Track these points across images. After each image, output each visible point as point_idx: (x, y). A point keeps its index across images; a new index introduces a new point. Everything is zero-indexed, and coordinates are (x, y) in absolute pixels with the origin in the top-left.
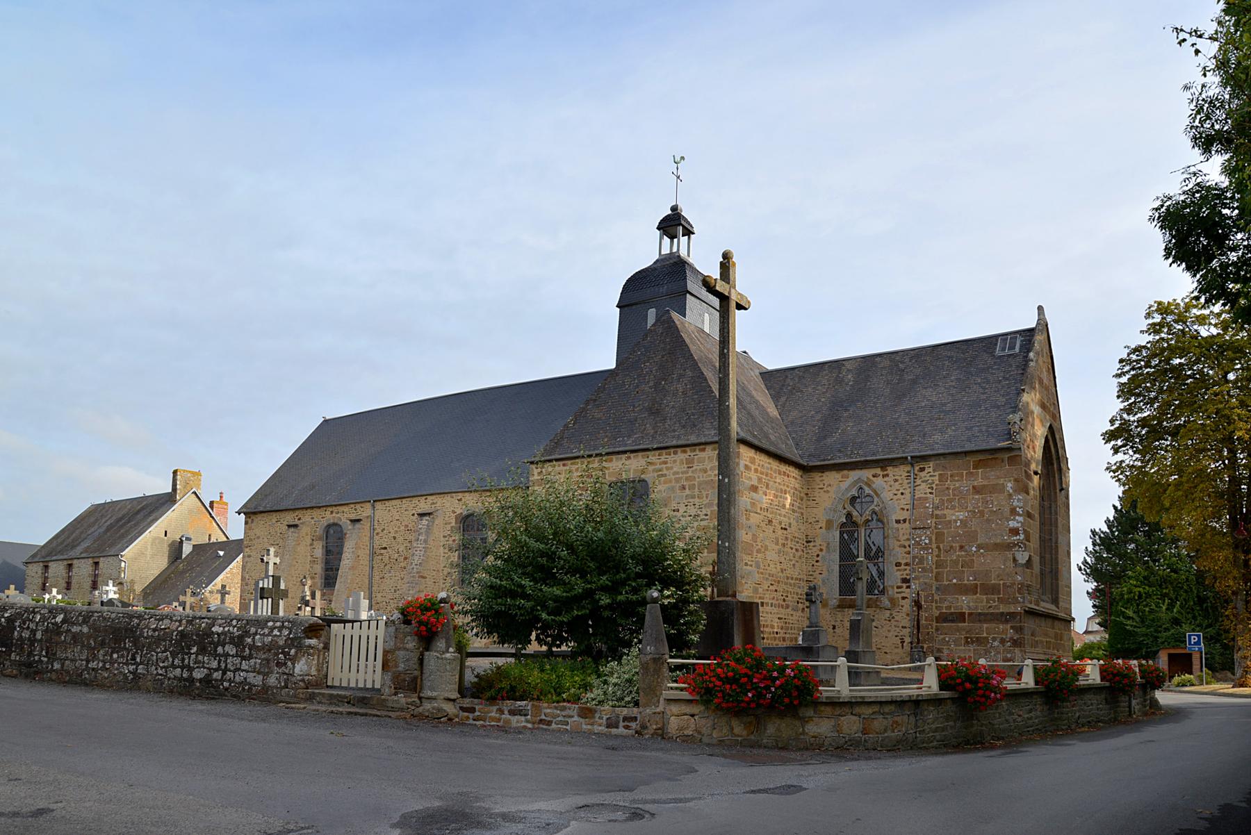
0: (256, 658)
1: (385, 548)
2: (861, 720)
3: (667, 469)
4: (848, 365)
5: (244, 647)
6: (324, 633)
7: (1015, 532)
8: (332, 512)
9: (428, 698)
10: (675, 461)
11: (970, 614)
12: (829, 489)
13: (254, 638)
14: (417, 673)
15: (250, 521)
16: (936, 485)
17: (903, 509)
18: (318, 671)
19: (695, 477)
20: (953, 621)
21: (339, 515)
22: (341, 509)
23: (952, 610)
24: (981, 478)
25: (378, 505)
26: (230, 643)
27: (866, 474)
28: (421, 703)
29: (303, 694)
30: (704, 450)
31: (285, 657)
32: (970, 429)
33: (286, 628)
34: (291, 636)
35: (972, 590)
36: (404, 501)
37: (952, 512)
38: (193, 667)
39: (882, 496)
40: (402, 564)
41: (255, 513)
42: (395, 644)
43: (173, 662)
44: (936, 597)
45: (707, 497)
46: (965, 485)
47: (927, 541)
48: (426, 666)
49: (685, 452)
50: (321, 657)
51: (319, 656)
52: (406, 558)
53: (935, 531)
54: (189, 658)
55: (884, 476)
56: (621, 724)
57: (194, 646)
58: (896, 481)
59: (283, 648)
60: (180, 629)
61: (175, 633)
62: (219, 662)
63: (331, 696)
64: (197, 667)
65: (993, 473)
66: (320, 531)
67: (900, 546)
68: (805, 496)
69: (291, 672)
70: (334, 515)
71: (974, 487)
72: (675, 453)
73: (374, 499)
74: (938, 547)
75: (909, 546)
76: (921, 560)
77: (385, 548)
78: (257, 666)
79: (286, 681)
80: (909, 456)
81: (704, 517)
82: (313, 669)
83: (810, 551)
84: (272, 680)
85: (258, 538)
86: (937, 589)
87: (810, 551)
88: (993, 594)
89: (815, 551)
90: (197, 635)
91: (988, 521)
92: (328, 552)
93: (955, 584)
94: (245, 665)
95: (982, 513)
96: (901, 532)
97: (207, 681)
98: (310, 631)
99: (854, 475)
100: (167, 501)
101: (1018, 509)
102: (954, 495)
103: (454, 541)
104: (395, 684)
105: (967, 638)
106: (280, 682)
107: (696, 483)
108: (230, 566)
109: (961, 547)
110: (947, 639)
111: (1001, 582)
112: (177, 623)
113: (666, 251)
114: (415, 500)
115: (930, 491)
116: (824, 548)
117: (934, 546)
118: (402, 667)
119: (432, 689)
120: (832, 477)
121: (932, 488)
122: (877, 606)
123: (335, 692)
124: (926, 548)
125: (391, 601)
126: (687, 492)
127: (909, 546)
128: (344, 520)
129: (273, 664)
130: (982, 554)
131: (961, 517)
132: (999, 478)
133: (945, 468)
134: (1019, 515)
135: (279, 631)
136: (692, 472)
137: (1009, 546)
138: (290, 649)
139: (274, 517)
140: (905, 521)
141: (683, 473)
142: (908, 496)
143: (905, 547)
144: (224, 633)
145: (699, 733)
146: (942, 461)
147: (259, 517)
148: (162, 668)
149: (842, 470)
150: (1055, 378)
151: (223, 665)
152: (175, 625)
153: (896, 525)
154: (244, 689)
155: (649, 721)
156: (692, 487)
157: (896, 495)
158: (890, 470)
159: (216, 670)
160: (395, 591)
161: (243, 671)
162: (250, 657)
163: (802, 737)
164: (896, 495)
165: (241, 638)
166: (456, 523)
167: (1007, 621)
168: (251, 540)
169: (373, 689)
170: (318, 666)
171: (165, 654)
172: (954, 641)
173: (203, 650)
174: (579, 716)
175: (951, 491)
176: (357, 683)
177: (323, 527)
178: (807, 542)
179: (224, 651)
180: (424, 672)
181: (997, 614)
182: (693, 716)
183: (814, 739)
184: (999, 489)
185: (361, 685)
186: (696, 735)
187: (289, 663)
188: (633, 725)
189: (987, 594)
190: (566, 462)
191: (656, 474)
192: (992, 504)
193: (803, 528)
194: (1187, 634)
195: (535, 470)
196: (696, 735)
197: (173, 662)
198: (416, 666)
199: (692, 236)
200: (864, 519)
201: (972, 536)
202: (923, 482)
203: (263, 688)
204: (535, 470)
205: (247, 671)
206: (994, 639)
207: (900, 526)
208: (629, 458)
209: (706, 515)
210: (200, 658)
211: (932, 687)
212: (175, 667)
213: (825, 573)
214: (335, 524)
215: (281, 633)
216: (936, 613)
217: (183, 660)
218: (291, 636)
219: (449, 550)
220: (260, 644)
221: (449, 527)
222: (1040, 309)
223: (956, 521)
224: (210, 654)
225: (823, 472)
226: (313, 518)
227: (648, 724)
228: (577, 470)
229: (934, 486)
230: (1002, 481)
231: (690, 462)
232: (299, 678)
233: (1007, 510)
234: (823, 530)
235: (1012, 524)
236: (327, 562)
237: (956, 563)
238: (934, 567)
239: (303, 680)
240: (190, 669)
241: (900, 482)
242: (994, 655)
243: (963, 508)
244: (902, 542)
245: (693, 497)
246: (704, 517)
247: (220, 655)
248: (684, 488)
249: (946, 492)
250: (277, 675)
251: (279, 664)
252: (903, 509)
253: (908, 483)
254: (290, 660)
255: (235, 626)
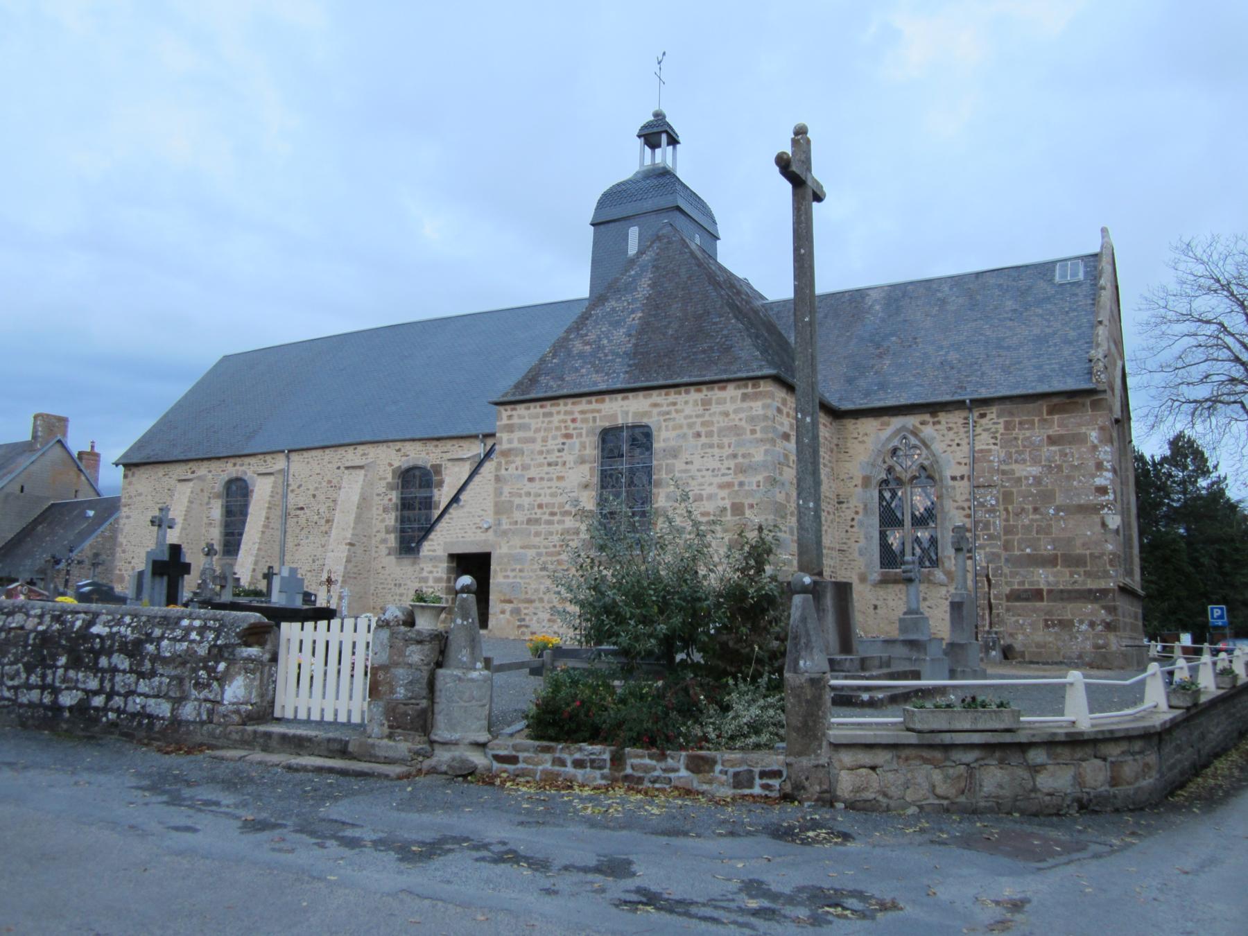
0: (162, 675)
1: (302, 509)
2: (1108, 765)
3: (677, 411)
4: (874, 295)
5: (143, 658)
6: (270, 638)
7: (1102, 490)
8: (235, 465)
9: (444, 744)
10: (686, 403)
11: (1050, 592)
12: (865, 438)
13: (158, 645)
14: (424, 703)
15: (130, 473)
16: (1002, 434)
17: (960, 463)
18: (262, 696)
19: (713, 422)
20: (1027, 599)
21: (243, 468)
22: (247, 460)
23: (1027, 586)
24: (1057, 425)
25: (294, 456)
26: (120, 651)
27: (912, 421)
28: (433, 750)
29: (237, 733)
30: (724, 388)
31: (209, 675)
32: (1040, 367)
33: (210, 628)
34: (219, 642)
35: (1051, 561)
36: (327, 451)
37: (1022, 467)
38: (60, 687)
39: (933, 447)
40: (323, 529)
41: (137, 465)
42: (390, 657)
43: (28, 679)
44: (1006, 570)
45: (729, 446)
46: (1038, 434)
47: (993, 502)
48: (441, 691)
49: (699, 391)
50: (266, 676)
51: (262, 673)
52: (328, 521)
53: (1002, 490)
54: (54, 673)
55: (934, 424)
56: (758, 781)
57: (62, 655)
58: (950, 429)
59: (205, 660)
60: (41, 628)
61: (32, 636)
62: (102, 681)
63: (284, 737)
64: (67, 688)
65: (1072, 420)
66: (219, 487)
67: (958, 508)
68: (835, 448)
69: (219, 698)
70: (237, 467)
71: (1049, 437)
72: (687, 392)
73: (289, 448)
74: (1006, 510)
75: (970, 508)
76: (987, 526)
77: (302, 509)
78: (164, 688)
79: (211, 712)
80: (967, 398)
81: (727, 471)
82: (254, 694)
83: (842, 514)
84: (188, 711)
85: (140, 495)
86: (1007, 560)
87: (842, 514)
88: (1077, 566)
89: (849, 514)
90: (69, 639)
91: (1068, 478)
92: (229, 512)
93: (1029, 555)
94: (143, 686)
95: (1059, 468)
96: (958, 491)
97: (81, 708)
98: (250, 634)
99: (897, 422)
100: (25, 451)
101: (1105, 463)
102: (1024, 446)
103: (390, 500)
104: (389, 721)
105: (1046, 621)
106: (199, 714)
107: (715, 429)
108: (102, 529)
109: (1036, 510)
110: (1021, 622)
111: (1088, 552)
112: (36, 620)
113: (648, 162)
114: (341, 451)
115: (993, 441)
116: (861, 510)
117: (1001, 508)
118: (401, 692)
119: (452, 727)
120: (869, 426)
121: (996, 438)
122: (929, 581)
123: (291, 731)
124: (992, 510)
125: (309, 574)
126: (703, 440)
127: (970, 508)
128: (250, 473)
129: (189, 685)
130: (1062, 517)
131: (1034, 473)
132: (1080, 425)
133: (1011, 414)
134: (1107, 470)
135: (198, 634)
136: (710, 415)
137: (1095, 509)
138: (217, 663)
139: (161, 470)
140: (962, 478)
141: (697, 416)
142: (965, 448)
143: (963, 509)
144: (112, 636)
145: (885, 795)
146: (1008, 406)
147: (142, 469)
148: (9, 688)
149: (881, 416)
150: (1119, 310)
151: (107, 686)
152: (30, 624)
153: (951, 483)
154: (140, 724)
155: (807, 779)
156: (709, 434)
157: (950, 446)
158: (942, 417)
159: (96, 693)
160: (314, 561)
161: (140, 695)
162: (153, 673)
163: (1033, 795)
164: (950, 446)
165: (138, 644)
166: (393, 478)
167: (1096, 600)
168: (130, 497)
169: (348, 724)
170: (261, 688)
171: (15, 667)
172: (1030, 625)
173: (76, 662)
174: (688, 768)
175: (1020, 442)
176: (336, 715)
177: (223, 483)
178: (840, 503)
179: (110, 663)
180: (437, 700)
181: (1084, 591)
182: (873, 768)
183: (1049, 798)
184: (1079, 439)
185: (342, 718)
186: (880, 798)
187: (215, 684)
188: (775, 783)
189: (1069, 566)
190: (544, 403)
191: (662, 418)
192: (1073, 457)
193: (834, 486)
194: (1210, 607)
195: (503, 412)
196: (880, 798)
197: (28, 679)
198: (424, 693)
199: (678, 146)
200: (909, 475)
201: (1047, 496)
202: (984, 430)
203: (172, 723)
204: (503, 412)
205: (146, 696)
206: (1081, 622)
207: (956, 483)
208: (627, 398)
209: (729, 469)
210: (71, 673)
211: (1160, 705)
212: (30, 688)
213: (862, 542)
214: (238, 479)
215: (202, 637)
216: (1007, 590)
217: (44, 677)
218: (219, 642)
219: (384, 511)
220: (168, 654)
221: (383, 483)
222: (1104, 231)
223: (1027, 478)
224: (88, 668)
225: (857, 419)
226: (210, 472)
227: (807, 784)
228: (559, 413)
229: (998, 435)
230: (1083, 430)
231: (706, 403)
232: (231, 708)
233: (1091, 464)
234: (859, 489)
235: (1099, 481)
236: (227, 525)
237: (1027, 529)
238: (1002, 533)
239: (238, 712)
240: (55, 691)
241: (955, 430)
242: (1082, 641)
243: (1035, 461)
244: (960, 504)
245: (711, 446)
246: (727, 471)
247: (103, 671)
248: (698, 435)
249: (1014, 443)
250: (196, 703)
251: (198, 685)
252: (960, 463)
253: (966, 432)
254: (217, 680)
255: (129, 625)
